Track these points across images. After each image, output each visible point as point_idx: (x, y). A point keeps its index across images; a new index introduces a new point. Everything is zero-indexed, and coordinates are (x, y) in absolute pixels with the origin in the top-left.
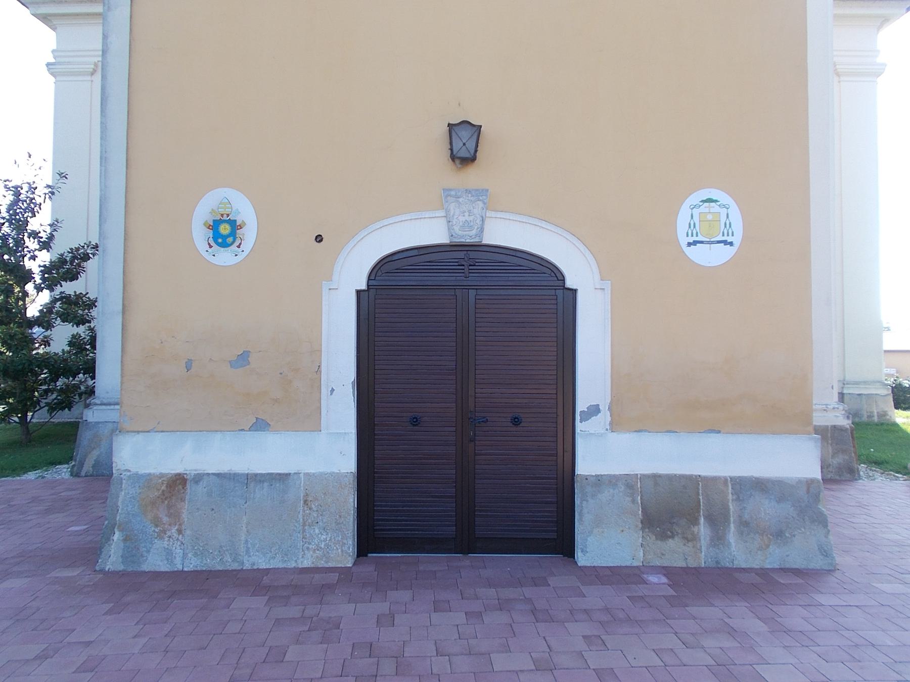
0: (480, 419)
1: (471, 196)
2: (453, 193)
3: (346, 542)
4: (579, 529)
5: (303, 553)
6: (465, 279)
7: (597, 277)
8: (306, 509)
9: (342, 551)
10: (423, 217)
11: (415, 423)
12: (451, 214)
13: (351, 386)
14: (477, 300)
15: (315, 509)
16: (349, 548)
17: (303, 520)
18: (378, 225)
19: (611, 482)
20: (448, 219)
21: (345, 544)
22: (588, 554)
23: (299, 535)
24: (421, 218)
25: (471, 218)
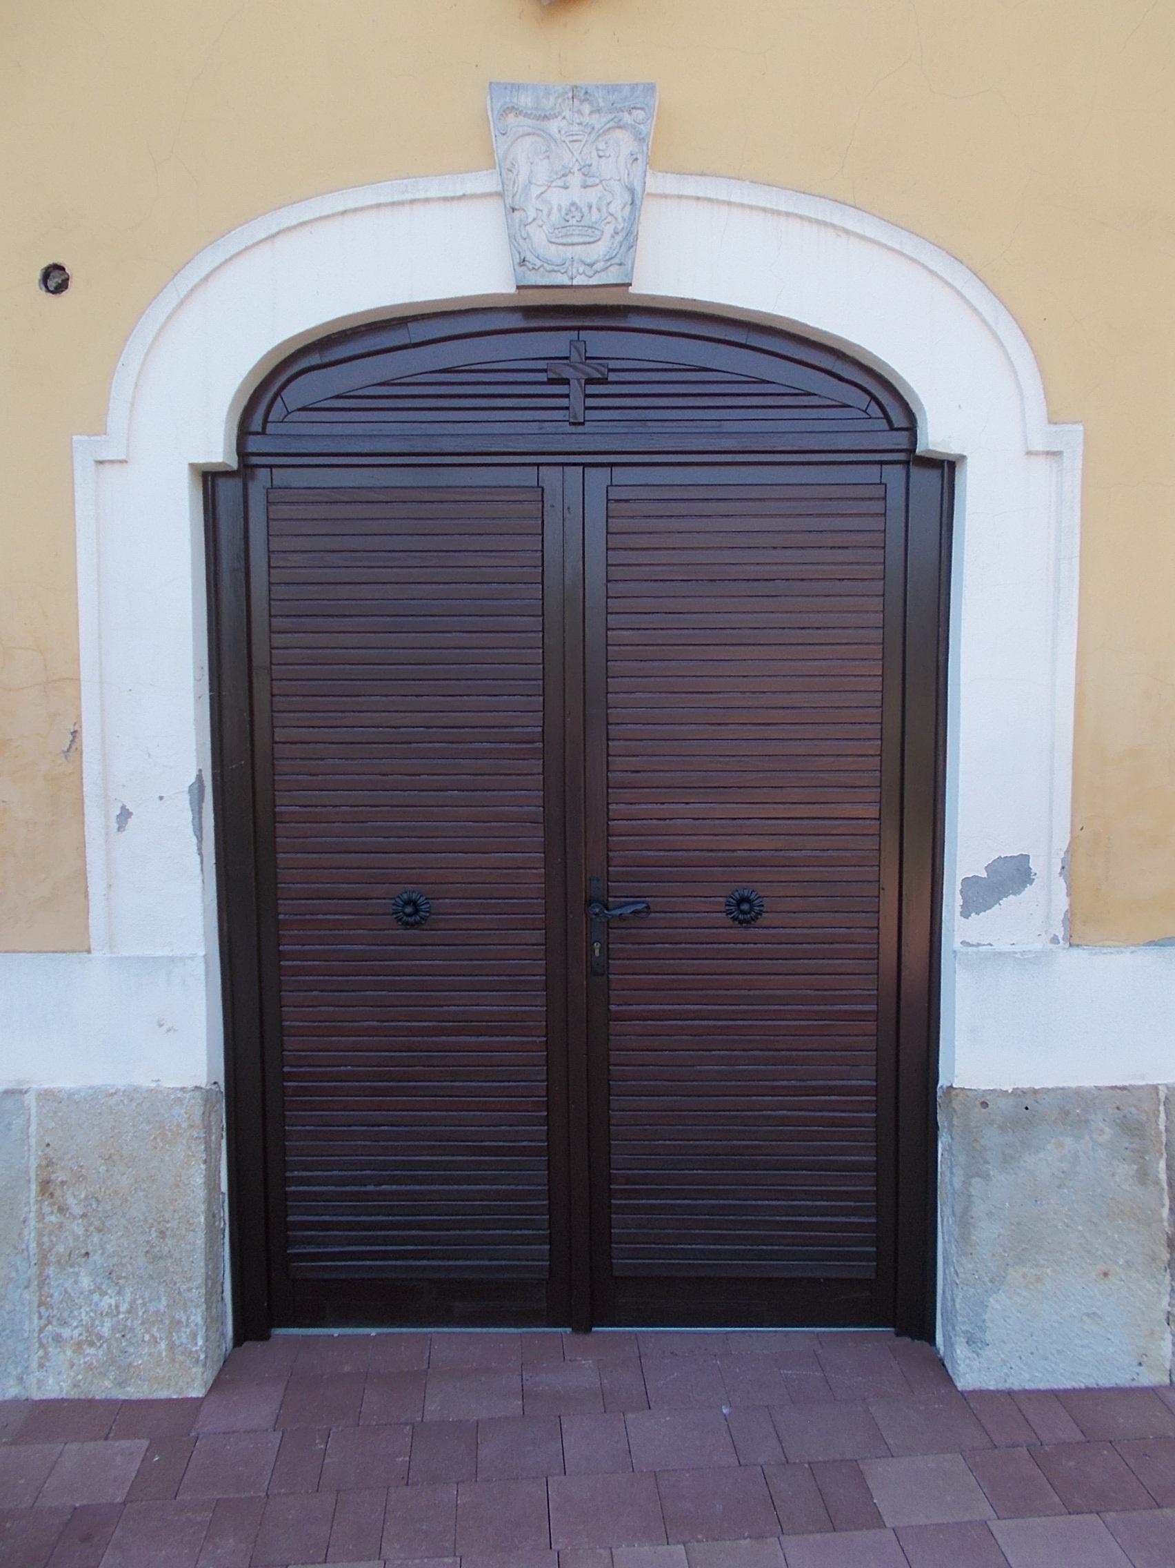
0: (627, 904)
1: (591, 113)
2: (525, 100)
3: (184, 1320)
4: (960, 1270)
5: (41, 1353)
6: (573, 429)
7: (1037, 409)
8: (46, 1209)
9: (172, 1347)
10: (422, 195)
11: (411, 920)
12: (522, 179)
13: (185, 801)
14: (612, 506)
15: (77, 1210)
16: (194, 1336)
17: (40, 1244)
18: (260, 228)
19: (1068, 1113)
20: (509, 201)
21: (179, 1322)
22: (988, 1352)
23: (26, 1296)
24: (412, 202)
25: (592, 195)
